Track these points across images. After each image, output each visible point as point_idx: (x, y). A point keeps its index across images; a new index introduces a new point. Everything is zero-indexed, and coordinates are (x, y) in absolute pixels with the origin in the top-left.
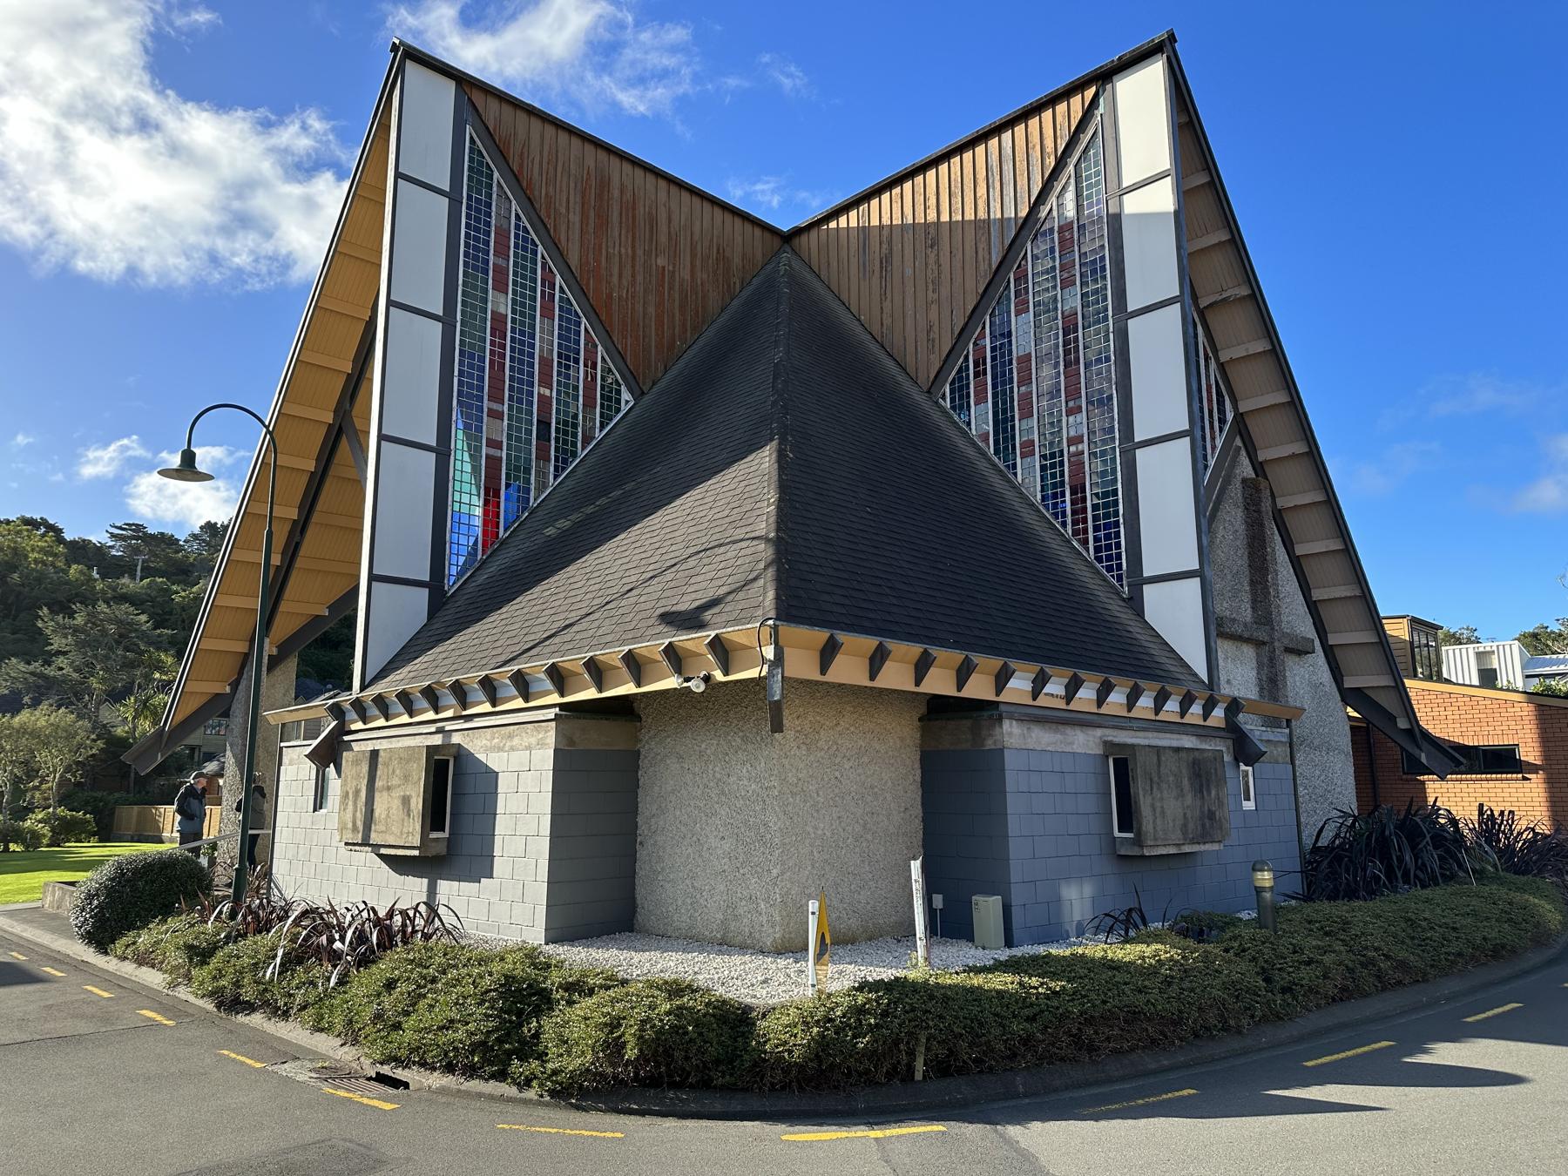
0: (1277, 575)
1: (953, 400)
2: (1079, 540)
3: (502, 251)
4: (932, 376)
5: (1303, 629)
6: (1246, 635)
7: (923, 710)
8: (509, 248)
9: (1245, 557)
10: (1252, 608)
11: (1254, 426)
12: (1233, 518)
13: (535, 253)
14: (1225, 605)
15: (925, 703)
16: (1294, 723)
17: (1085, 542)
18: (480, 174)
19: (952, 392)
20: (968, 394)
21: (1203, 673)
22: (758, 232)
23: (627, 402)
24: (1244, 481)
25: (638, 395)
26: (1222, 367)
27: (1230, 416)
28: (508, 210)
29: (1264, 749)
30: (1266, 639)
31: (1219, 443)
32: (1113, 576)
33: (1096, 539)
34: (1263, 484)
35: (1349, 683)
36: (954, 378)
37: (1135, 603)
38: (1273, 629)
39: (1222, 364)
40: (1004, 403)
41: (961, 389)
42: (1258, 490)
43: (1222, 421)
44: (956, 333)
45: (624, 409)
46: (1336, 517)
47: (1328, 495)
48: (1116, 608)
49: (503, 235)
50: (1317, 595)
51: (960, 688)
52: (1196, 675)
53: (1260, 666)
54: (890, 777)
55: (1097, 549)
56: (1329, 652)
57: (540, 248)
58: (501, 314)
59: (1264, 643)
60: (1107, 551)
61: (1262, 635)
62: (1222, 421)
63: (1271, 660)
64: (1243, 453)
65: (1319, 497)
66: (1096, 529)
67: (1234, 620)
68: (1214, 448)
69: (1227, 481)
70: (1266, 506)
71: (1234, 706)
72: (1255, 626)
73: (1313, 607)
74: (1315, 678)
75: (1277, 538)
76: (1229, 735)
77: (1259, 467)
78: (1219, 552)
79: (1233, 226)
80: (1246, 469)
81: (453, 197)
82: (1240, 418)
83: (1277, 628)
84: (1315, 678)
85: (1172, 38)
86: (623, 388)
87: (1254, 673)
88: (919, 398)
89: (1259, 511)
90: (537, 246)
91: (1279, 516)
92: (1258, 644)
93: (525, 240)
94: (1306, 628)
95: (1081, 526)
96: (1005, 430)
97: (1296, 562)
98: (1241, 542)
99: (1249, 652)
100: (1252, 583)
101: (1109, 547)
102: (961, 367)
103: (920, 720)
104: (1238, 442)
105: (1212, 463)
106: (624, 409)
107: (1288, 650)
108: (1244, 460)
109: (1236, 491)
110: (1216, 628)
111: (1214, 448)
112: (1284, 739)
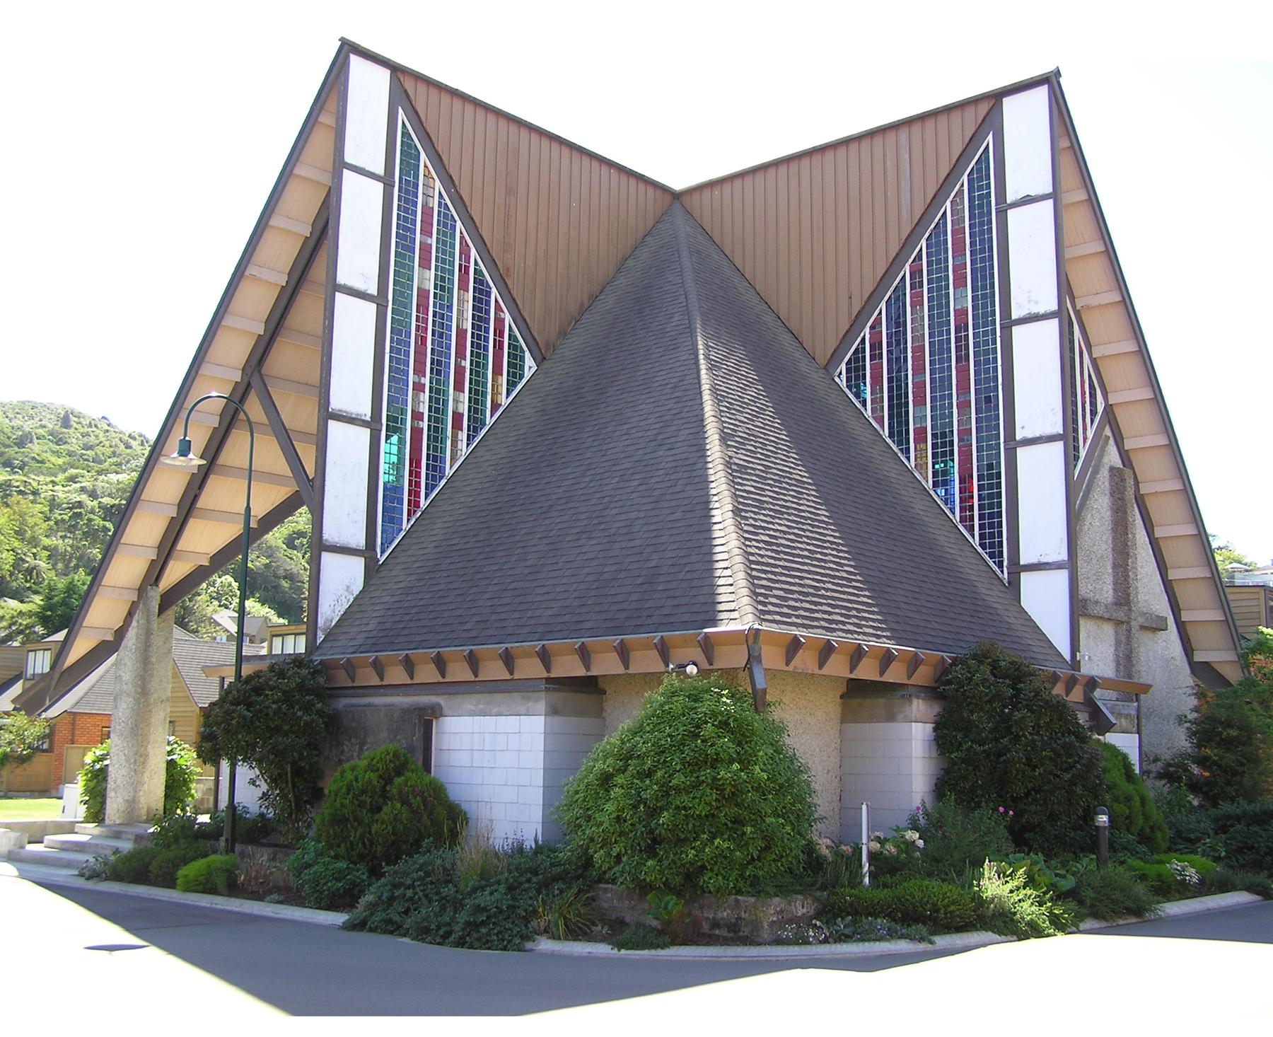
0: (1136, 558)
1: (848, 379)
2: (965, 527)
3: (426, 231)
4: (829, 356)
5: (1157, 607)
6: (1106, 615)
7: (843, 688)
8: (432, 225)
9: (1110, 542)
10: (1114, 589)
11: (1121, 416)
12: (1100, 505)
13: (454, 228)
14: (1090, 587)
15: (845, 683)
16: (1142, 696)
17: (971, 530)
18: (410, 157)
19: (848, 371)
20: (864, 375)
21: (1066, 653)
22: (650, 190)
23: (530, 368)
24: (1112, 469)
25: (540, 360)
26: (1094, 361)
27: (1100, 408)
28: (432, 191)
29: (1114, 722)
30: (1125, 619)
31: (1090, 434)
32: (994, 562)
33: (981, 527)
34: (1128, 472)
35: (1199, 657)
36: (850, 359)
37: (1014, 586)
38: (1130, 610)
39: (1095, 359)
40: (899, 387)
41: (857, 369)
42: (1123, 480)
43: (1094, 413)
44: (854, 315)
45: (528, 374)
46: (1191, 506)
47: (1184, 485)
48: (994, 596)
49: (427, 212)
50: (1172, 575)
51: (882, 673)
52: (1060, 655)
53: (1118, 643)
54: (818, 745)
55: (982, 536)
56: (1181, 627)
57: (459, 224)
58: (426, 290)
59: (1122, 622)
60: (991, 540)
61: (1121, 615)
62: (1094, 413)
63: (1129, 637)
64: (1112, 442)
65: (1177, 486)
66: (981, 517)
67: (1096, 602)
68: (1085, 439)
69: (1096, 471)
70: (1130, 493)
71: (1092, 683)
72: (1115, 607)
73: (1168, 585)
74: (1167, 653)
75: (1139, 522)
76: (1087, 709)
77: (1125, 456)
78: (1087, 539)
79: (1107, 239)
80: (1112, 457)
81: (387, 181)
82: (1109, 408)
83: (1134, 608)
84: (1167, 653)
85: (1057, 73)
86: (527, 354)
87: (1113, 649)
88: (816, 377)
89: (1122, 499)
90: (455, 222)
91: (1140, 500)
92: (1118, 623)
93: (446, 216)
94: (1162, 607)
95: (968, 513)
96: (899, 415)
97: (1154, 543)
98: (1107, 525)
99: (1108, 630)
100: (1115, 566)
101: (992, 536)
102: (857, 349)
103: (841, 697)
104: (1108, 431)
105: (1083, 453)
106: (528, 374)
107: (1143, 628)
108: (1112, 450)
109: (1103, 478)
110: (1079, 608)
111: (1085, 439)
112: (1133, 712)
